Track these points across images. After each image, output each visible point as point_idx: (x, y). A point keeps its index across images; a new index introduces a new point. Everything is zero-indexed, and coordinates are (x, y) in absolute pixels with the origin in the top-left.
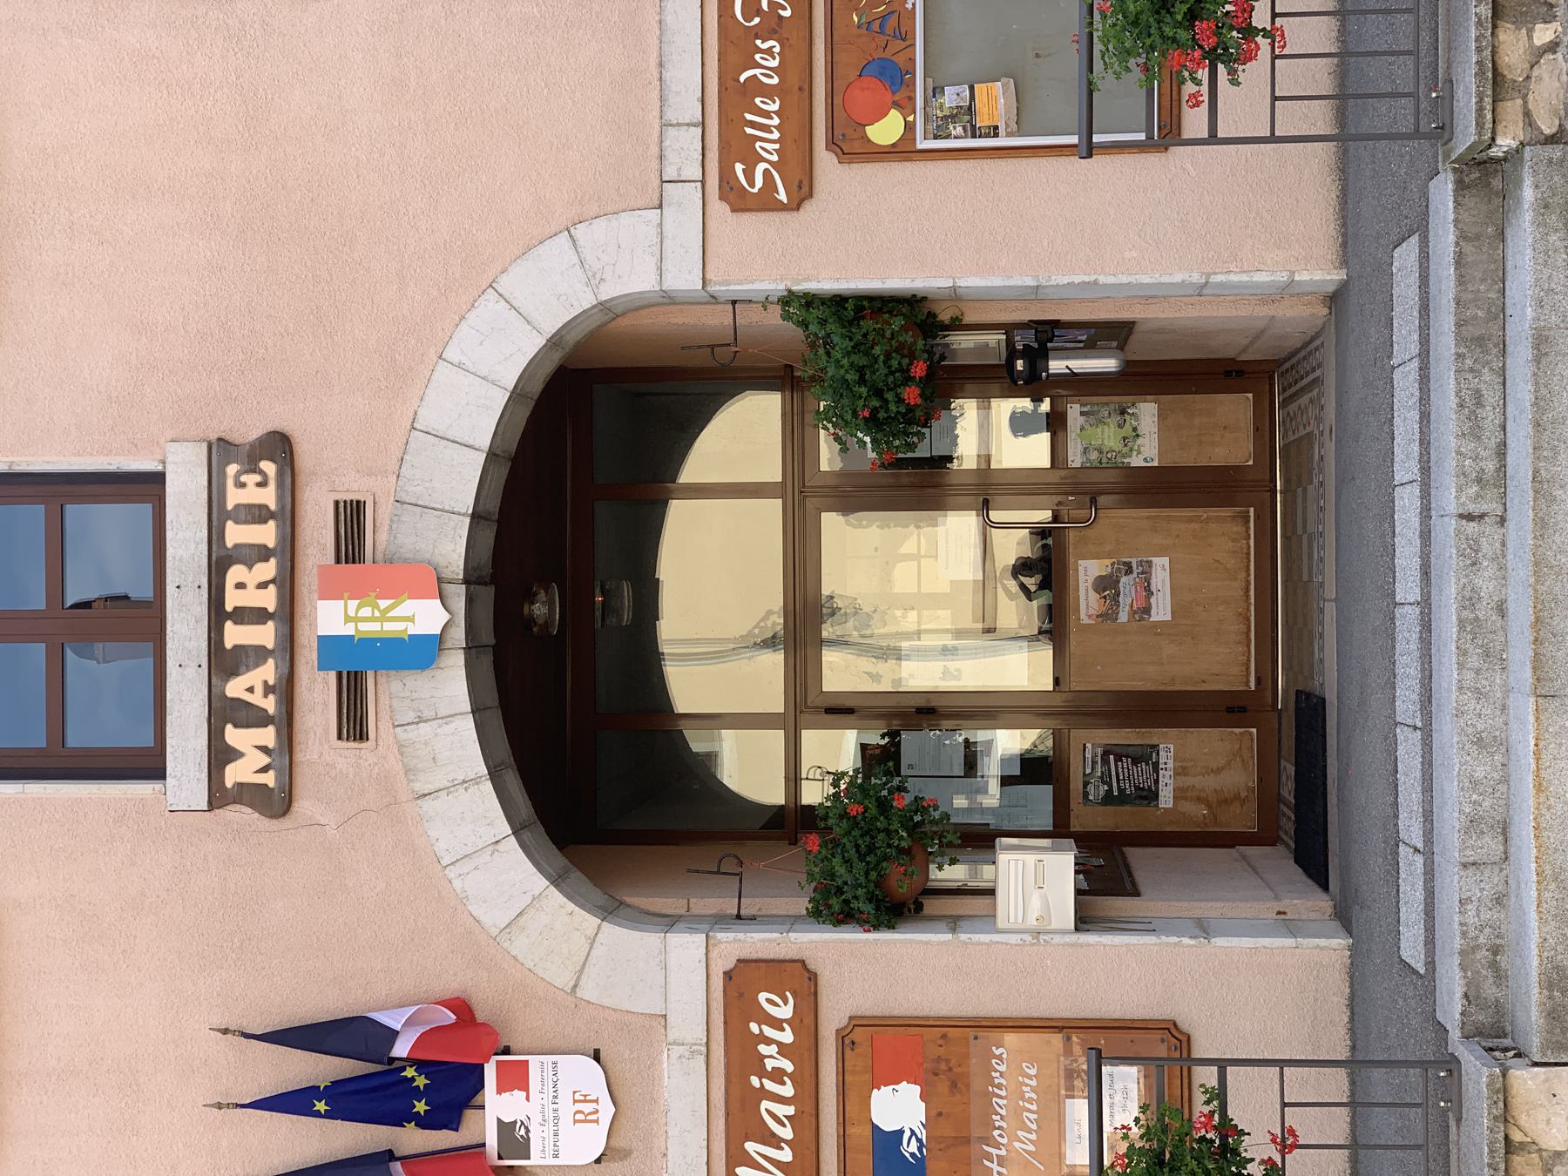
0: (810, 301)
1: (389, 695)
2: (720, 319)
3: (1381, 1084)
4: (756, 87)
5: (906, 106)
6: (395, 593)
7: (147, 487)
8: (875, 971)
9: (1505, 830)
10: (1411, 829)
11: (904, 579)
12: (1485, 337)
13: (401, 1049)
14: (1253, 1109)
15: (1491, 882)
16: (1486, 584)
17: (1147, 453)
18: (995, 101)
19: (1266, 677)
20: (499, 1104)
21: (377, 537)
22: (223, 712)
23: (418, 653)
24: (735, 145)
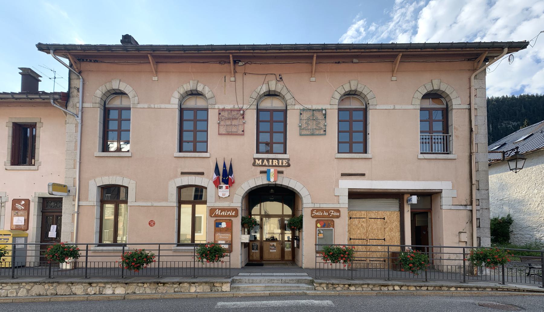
0: (302, 217)
1: (264, 176)
2: (300, 209)
3: (228, 271)
4: (323, 213)
5: (321, 227)
6: (274, 177)
7: (285, 152)
8: (237, 223)
9: (252, 283)
10: (252, 274)
11: (272, 225)
12: (299, 281)
13: (230, 177)
14: (225, 259)
15: (247, 281)
16: (275, 281)
17: (286, 250)
18: (321, 236)
19: (265, 261)
20: (224, 186)
21: (280, 175)
22: (263, 160)
23: (269, 179)
24: (318, 210)
